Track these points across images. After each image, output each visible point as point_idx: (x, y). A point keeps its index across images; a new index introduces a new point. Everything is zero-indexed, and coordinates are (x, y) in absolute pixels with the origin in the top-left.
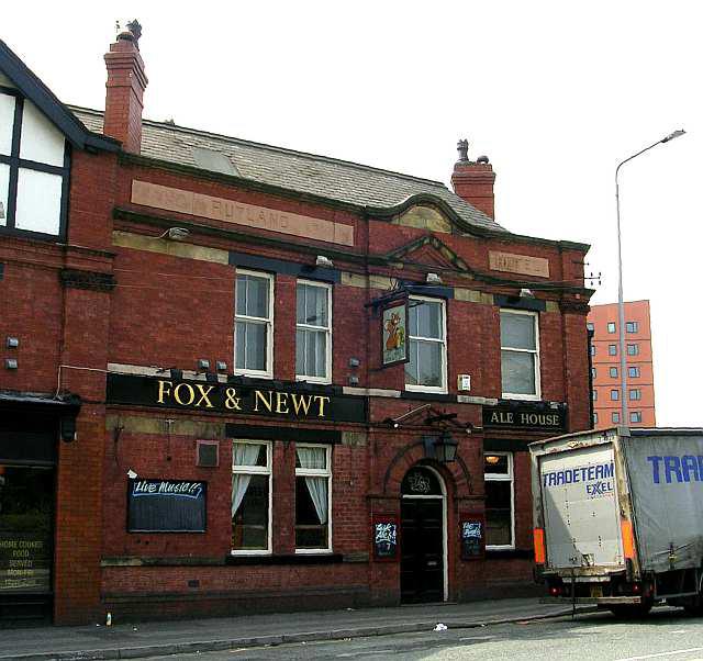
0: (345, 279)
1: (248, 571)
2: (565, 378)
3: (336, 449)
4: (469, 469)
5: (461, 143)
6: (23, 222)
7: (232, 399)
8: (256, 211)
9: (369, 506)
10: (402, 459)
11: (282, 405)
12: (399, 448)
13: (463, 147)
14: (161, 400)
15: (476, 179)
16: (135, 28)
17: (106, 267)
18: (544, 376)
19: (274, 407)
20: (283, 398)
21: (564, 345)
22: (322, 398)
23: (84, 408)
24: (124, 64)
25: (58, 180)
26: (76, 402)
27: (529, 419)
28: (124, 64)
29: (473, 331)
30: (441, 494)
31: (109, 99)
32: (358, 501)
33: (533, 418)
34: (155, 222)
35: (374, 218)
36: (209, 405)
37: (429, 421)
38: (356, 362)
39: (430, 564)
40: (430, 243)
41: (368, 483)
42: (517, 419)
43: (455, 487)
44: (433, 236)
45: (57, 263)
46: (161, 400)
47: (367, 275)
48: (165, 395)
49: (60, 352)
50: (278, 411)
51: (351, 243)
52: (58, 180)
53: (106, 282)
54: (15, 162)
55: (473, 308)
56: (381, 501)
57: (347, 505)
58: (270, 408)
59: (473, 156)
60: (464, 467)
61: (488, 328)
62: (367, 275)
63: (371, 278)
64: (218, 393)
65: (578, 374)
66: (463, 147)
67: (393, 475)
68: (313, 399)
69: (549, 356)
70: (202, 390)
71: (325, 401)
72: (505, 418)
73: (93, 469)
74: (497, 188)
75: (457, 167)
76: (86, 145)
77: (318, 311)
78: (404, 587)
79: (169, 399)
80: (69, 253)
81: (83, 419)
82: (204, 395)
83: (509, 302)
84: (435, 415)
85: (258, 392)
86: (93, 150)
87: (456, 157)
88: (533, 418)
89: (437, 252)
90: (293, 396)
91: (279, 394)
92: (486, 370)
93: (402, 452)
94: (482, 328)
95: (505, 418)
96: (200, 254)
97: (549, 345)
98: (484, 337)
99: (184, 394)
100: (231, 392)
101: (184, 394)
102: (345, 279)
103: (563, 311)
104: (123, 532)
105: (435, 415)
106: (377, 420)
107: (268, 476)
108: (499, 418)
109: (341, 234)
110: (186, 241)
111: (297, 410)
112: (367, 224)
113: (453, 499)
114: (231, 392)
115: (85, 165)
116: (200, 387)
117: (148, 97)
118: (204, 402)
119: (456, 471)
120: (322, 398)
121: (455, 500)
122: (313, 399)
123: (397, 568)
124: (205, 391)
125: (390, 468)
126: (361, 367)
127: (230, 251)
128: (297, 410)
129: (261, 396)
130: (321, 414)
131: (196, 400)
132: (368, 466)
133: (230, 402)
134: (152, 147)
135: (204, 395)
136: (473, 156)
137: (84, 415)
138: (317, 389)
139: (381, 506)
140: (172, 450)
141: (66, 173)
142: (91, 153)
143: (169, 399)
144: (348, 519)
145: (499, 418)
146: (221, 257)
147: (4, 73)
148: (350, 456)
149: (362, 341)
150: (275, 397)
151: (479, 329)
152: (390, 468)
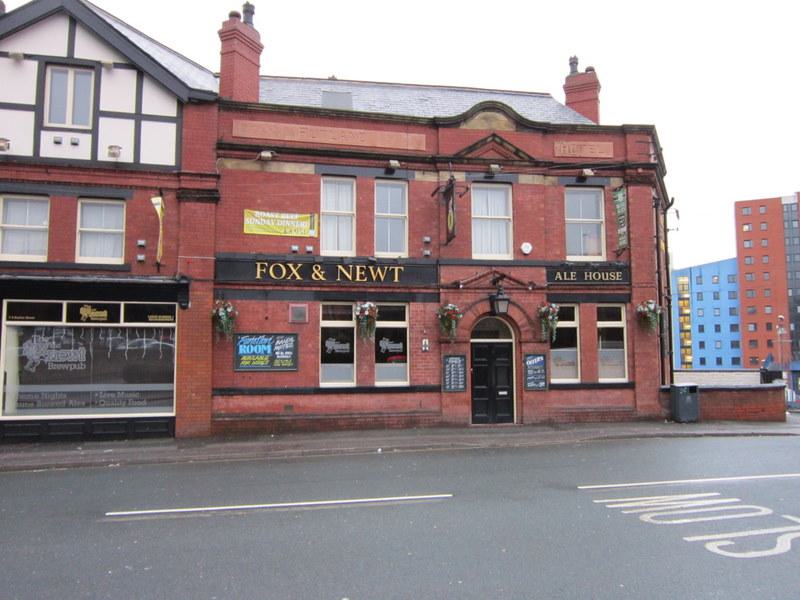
5: (571, 59)
6: (147, 158)
7: (318, 274)
8: (387, 134)
13: (574, 62)
15: (583, 87)
16: (249, 10)
17: (210, 185)
19: (354, 277)
23: (194, 285)
24: (238, 37)
27: (592, 276)
28: (238, 37)
30: (511, 338)
31: (223, 63)
33: (597, 275)
34: (250, 150)
35: (444, 126)
36: (298, 278)
37: (495, 282)
38: (427, 239)
39: (501, 393)
40: (493, 140)
42: (580, 276)
45: (174, 185)
46: (258, 276)
48: (262, 272)
49: (178, 246)
50: (358, 279)
53: (212, 197)
54: (138, 117)
58: (350, 277)
59: (581, 69)
64: (306, 271)
66: (574, 62)
70: (292, 268)
71: (399, 270)
74: (602, 96)
75: (568, 79)
76: (190, 99)
77: (392, 201)
78: (474, 410)
79: (266, 275)
80: (182, 177)
82: (294, 271)
83: (578, 181)
85: (340, 267)
87: (567, 71)
88: (597, 275)
89: (501, 148)
90: (371, 268)
91: (358, 267)
96: (289, 168)
99: (278, 271)
100: (317, 268)
101: (278, 271)
107: (353, 329)
108: (563, 277)
109: (414, 142)
110: (273, 159)
111: (379, 270)
113: (520, 343)
114: (317, 268)
115: (192, 113)
116: (291, 265)
117: (263, 58)
118: (294, 276)
120: (396, 269)
121: (520, 343)
123: (239, 302)
124: (295, 267)
126: (434, 243)
128: (374, 278)
129: (347, 274)
130: (396, 280)
131: (287, 276)
133: (316, 275)
134: (267, 96)
135: (294, 271)
136: (581, 69)
141: (178, 120)
143: (266, 275)
145: (563, 277)
146: (308, 169)
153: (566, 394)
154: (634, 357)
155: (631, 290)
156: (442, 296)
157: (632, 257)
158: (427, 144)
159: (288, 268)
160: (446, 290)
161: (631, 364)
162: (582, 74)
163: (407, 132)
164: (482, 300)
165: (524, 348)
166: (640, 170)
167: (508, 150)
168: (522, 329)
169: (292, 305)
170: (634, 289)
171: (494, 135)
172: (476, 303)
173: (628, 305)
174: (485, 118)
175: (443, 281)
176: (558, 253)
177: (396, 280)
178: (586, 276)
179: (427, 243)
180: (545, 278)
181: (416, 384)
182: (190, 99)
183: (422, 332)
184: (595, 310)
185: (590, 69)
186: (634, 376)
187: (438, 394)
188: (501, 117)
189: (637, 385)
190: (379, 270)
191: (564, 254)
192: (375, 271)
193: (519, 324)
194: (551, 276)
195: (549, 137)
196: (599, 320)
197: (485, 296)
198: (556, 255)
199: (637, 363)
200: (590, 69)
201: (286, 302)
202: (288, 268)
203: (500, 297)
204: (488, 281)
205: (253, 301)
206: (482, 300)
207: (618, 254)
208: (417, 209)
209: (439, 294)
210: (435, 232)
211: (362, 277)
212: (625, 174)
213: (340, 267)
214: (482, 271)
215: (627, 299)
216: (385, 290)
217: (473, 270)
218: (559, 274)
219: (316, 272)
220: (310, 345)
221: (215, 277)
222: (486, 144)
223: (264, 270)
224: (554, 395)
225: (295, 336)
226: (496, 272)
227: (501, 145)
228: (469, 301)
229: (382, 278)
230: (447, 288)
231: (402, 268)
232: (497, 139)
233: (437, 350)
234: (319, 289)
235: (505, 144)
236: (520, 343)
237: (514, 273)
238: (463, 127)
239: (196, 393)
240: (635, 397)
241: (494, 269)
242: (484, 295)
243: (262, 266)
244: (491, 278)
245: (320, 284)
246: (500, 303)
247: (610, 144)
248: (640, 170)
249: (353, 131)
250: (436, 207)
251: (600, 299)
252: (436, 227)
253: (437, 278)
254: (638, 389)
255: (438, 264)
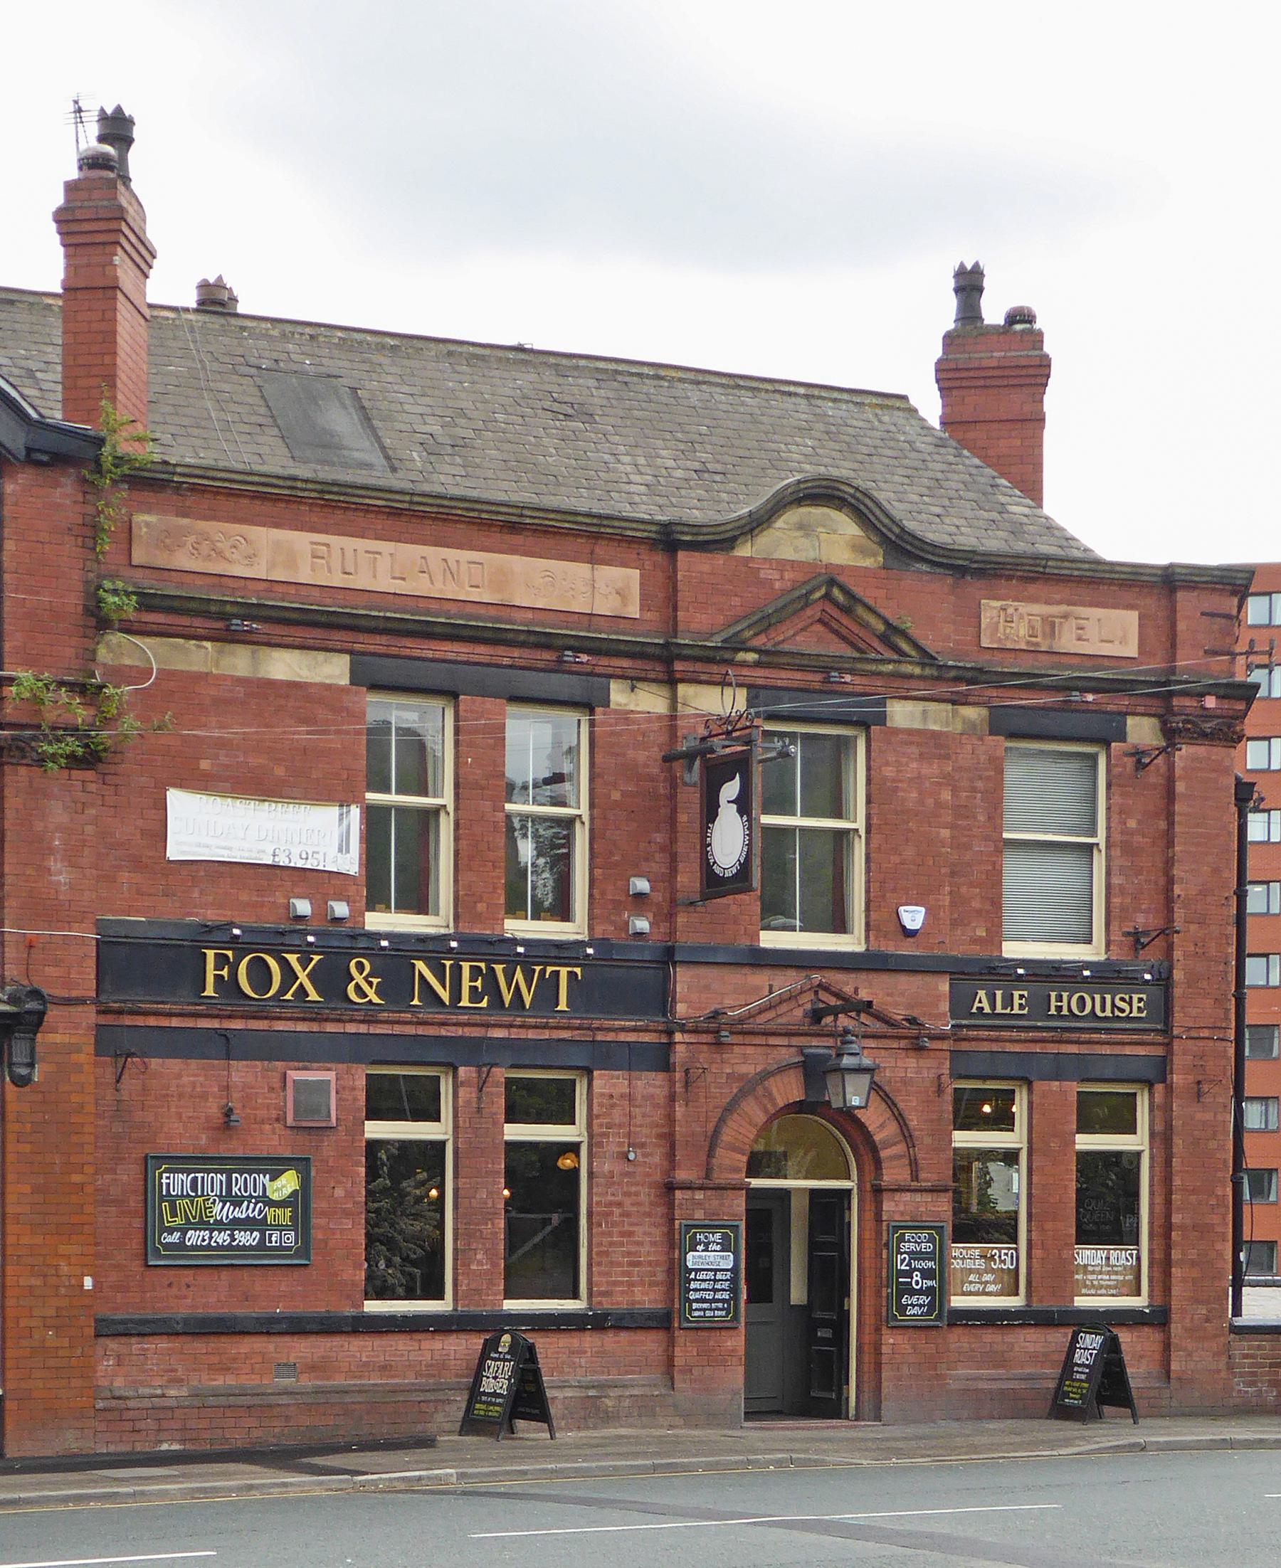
0: (619, 695)
1: (401, 1345)
2: (1169, 900)
3: (596, 1083)
4: (913, 1123)
9: (671, 1205)
10: (751, 1100)
11: (473, 989)
12: (742, 1077)
14: (209, 991)
18: (1116, 900)
19: (456, 995)
20: (475, 972)
21: (1171, 824)
22: (564, 971)
23: (53, 1014)
25: (1265, 911)
26: (32, 1005)
29: (930, 802)
32: (646, 1195)
36: (313, 996)
37: (816, 1016)
38: (642, 885)
40: (828, 596)
41: (671, 1155)
43: (878, 1163)
44: (831, 579)
46: (209, 991)
47: (671, 682)
48: (219, 978)
50: (465, 1002)
51: (634, 611)
52: (1265, 911)
55: (932, 745)
56: (699, 1195)
57: (619, 1204)
58: (445, 995)
59: (993, 312)
60: (900, 1119)
61: (974, 790)
62: (671, 682)
63: (682, 689)
65: (1203, 893)
67: (727, 1136)
68: (543, 972)
69: (1129, 850)
71: (572, 975)
72: (1008, 1001)
73: (75, 1139)
74: (1054, 400)
79: (229, 987)
81: (57, 1038)
82: (303, 977)
84: (833, 1001)
85: (420, 965)
86: (45, 458)
89: (845, 620)
90: (499, 968)
91: (466, 966)
92: (964, 890)
93: (750, 1087)
94: (955, 791)
95: (1008, 1001)
97: (1132, 824)
98: (962, 811)
99: (260, 975)
100: (360, 967)
101: (260, 975)
102: (619, 695)
103: (1171, 735)
104: (136, 1266)
105: (833, 1001)
106: (692, 1013)
108: (993, 1005)
111: (519, 975)
112: (674, 561)
114: (360, 967)
116: (292, 958)
119: (882, 1126)
120: (564, 971)
122: (543, 972)
124: (304, 963)
125: (722, 1120)
126: (658, 897)
127: (351, 652)
128: (507, 998)
130: (563, 1006)
131: (284, 989)
132: (671, 1119)
133: (358, 987)
135: (303, 977)
136: (993, 312)
137: (54, 1031)
138: (554, 953)
139: (700, 1204)
140: (235, 1095)
142: (40, 464)
143: (229, 987)
144: (622, 1234)
145: (993, 1005)
147: (3, 378)
148: (630, 1097)
149: (659, 837)
150: (457, 970)
151: (946, 795)
152: (722, 1120)
153: (990, 1337)
154: (1167, 1236)
155: (1168, 1045)
156: (680, 1053)
157: (1177, 954)
158: (644, 597)
159: (285, 965)
160: (688, 1038)
161: (1159, 1255)
162: (995, 327)
163: (593, 560)
164: (782, 1069)
165: (887, 1206)
166: (1210, 702)
167: (865, 626)
168: (883, 1154)
169: (294, 1075)
170: (1176, 1044)
171: (832, 582)
172: (771, 1074)
173: (1159, 1088)
174: (801, 527)
175: (681, 1009)
176: (981, 933)
177: (563, 1006)
178: (1053, 1003)
179: (640, 896)
180: (945, 1006)
181: (606, 1304)
182: (29, 450)
183: (625, 1156)
184: (1074, 1098)
185: (1020, 317)
186: (1167, 1290)
187: (661, 1335)
188: (847, 527)
189: (1174, 1317)
190: (519, 975)
191: (995, 937)
192: (509, 977)
193: (877, 1138)
194: (960, 1005)
195: (973, 586)
196: (1081, 1130)
197: (792, 1057)
198: (976, 941)
199: (1176, 1255)
200: (1020, 317)
201: (279, 1064)
202: (285, 965)
203: (847, 1061)
204: (799, 1013)
205: (194, 1063)
206: (782, 1069)
207: (1137, 940)
208: (616, 796)
209: (671, 1045)
210: (658, 865)
211: (475, 995)
212: (1170, 710)
213: (420, 965)
214: (786, 981)
215: (1156, 1075)
216: (531, 1034)
217: (760, 979)
218: (982, 994)
219: (359, 978)
220: (339, 1192)
221: (98, 991)
222: (807, 605)
223: (225, 973)
224: (958, 1339)
225: (301, 1165)
226: (825, 988)
227: (847, 611)
228: (749, 1069)
229: (528, 999)
230: (695, 1031)
231: (578, 970)
232: (836, 592)
233: (660, 1210)
234: (363, 1029)
235: (860, 611)
236: (878, 1191)
237: (866, 988)
238: (744, 550)
239: (56, 1328)
240: (1167, 1347)
241: (817, 977)
242: (785, 1053)
243: (221, 961)
244: (807, 1001)
245: (369, 1014)
246: (849, 1078)
247: (1131, 618)
248: (1210, 702)
249: (452, 554)
250: (662, 789)
251: (1081, 1069)
252: (663, 849)
253: (663, 1000)
254: (1176, 1328)
255: (668, 957)
